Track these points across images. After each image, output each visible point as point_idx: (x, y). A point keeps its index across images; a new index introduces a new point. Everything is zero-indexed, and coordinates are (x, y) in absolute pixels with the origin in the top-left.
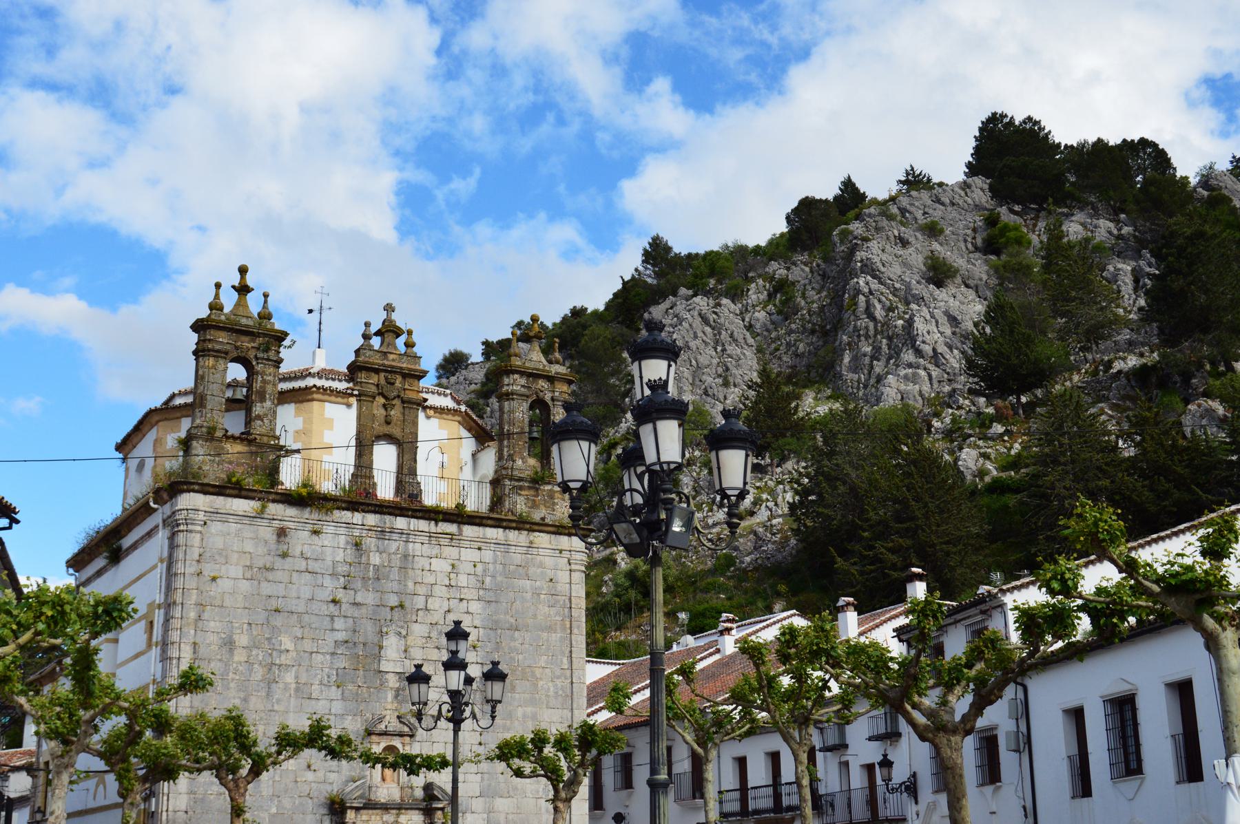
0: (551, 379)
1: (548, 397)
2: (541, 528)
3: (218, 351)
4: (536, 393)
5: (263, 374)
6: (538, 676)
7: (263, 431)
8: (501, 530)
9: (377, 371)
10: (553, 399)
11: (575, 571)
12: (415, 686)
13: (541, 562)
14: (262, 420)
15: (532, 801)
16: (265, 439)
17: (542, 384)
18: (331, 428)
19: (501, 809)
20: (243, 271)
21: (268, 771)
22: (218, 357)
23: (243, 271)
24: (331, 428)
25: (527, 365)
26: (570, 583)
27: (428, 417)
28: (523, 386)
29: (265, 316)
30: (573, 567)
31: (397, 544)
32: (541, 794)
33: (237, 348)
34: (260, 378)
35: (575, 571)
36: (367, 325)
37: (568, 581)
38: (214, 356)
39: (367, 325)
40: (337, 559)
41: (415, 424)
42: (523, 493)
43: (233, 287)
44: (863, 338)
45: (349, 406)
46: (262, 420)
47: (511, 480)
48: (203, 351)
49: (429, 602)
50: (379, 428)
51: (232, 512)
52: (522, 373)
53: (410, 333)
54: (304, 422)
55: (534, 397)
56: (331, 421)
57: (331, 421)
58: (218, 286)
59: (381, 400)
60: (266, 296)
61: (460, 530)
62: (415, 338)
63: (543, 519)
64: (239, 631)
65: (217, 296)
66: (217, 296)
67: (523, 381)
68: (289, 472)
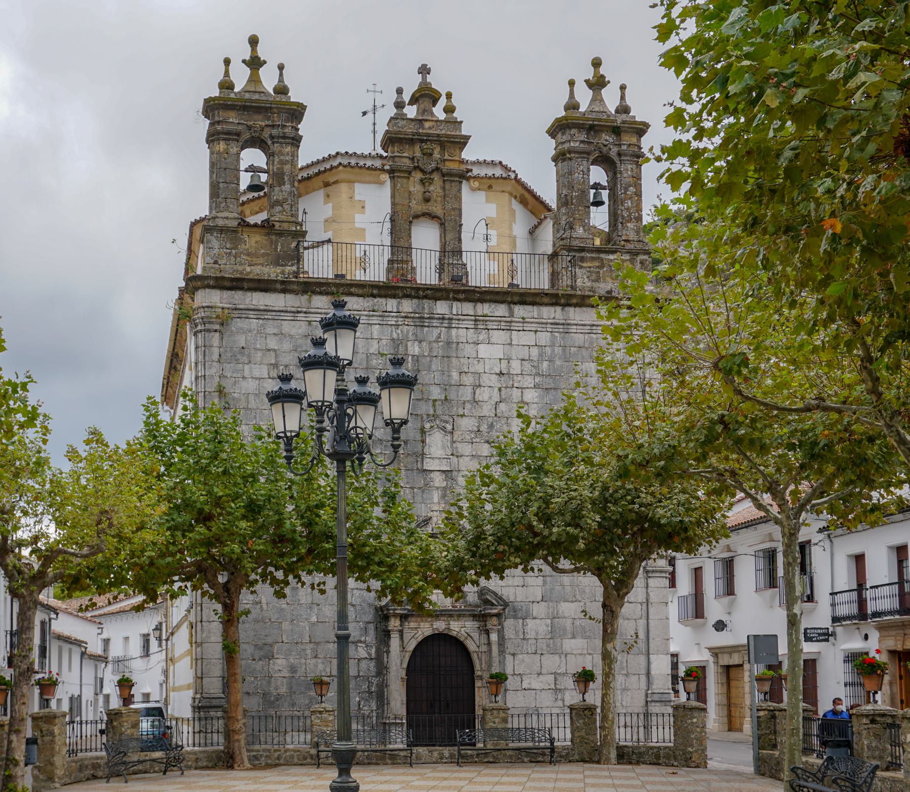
19: (566, 615)
36: (400, 91)
38: (225, 139)
39: (400, 91)
43: (244, 61)
50: (417, 206)
53: (449, 96)
60: (281, 67)
62: (454, 101)
65: (227, 74)
66: (227, 74)
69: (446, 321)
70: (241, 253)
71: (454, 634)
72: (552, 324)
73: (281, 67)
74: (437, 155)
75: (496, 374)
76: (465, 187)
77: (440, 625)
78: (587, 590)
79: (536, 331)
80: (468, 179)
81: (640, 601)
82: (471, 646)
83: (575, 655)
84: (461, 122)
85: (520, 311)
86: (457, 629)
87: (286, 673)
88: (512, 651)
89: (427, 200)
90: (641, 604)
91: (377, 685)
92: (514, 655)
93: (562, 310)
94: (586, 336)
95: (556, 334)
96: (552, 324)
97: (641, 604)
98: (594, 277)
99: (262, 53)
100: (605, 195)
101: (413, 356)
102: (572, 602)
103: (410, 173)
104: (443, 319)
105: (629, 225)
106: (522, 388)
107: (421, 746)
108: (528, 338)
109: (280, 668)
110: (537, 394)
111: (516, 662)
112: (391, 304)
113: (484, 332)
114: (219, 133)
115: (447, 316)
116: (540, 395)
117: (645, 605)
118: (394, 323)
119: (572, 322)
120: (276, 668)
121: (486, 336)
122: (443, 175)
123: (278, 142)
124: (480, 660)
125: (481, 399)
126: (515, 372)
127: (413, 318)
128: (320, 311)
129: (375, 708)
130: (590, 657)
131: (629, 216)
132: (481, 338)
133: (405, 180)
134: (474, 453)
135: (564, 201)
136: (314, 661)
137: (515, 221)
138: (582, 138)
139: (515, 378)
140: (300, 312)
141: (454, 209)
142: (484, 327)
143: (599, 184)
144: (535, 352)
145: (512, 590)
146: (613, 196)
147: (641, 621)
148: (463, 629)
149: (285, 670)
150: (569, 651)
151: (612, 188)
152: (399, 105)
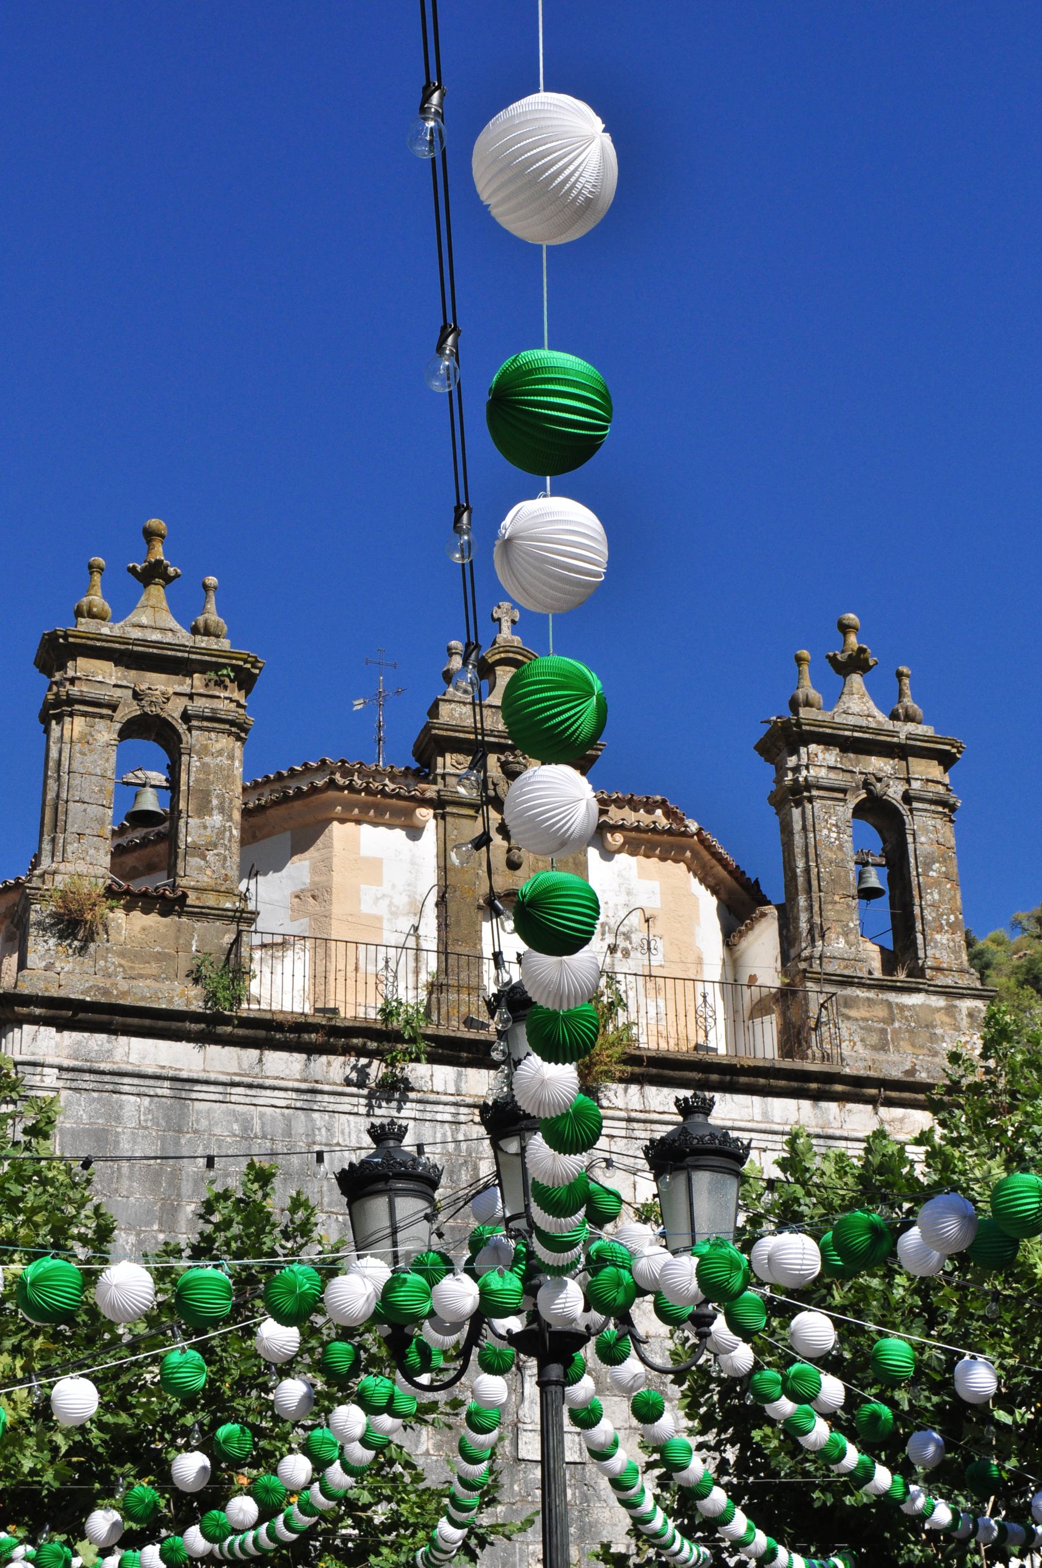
0: (900, 751)
1: (895, 792)
2: (976, 992)
4: (866, 785)
5: (205, 750)
7: (205, 879)
8: (806, 1104)
10: (907, 798)
12: (332, 1006)
14: (204, 857)
16: (211, 900)
21: (1035, 1265)
22: (94, 715)
25: (837, 720)
33: (137, 696)
34: (195, 762)
38: (85, 714)
42: (853, 1013)
45: (415, 832)
46: (204, 857)
47: (817, 981)
48: (58, 703)
51: (129, 1068)
52: (827, 740)
54: (314, 870)
55: (863, 794)
63: (912, 1072)
67: (831, 756)
68: (288, 987)
98: (874, 1039)
105: (938, 937)
118: (448, 1117)
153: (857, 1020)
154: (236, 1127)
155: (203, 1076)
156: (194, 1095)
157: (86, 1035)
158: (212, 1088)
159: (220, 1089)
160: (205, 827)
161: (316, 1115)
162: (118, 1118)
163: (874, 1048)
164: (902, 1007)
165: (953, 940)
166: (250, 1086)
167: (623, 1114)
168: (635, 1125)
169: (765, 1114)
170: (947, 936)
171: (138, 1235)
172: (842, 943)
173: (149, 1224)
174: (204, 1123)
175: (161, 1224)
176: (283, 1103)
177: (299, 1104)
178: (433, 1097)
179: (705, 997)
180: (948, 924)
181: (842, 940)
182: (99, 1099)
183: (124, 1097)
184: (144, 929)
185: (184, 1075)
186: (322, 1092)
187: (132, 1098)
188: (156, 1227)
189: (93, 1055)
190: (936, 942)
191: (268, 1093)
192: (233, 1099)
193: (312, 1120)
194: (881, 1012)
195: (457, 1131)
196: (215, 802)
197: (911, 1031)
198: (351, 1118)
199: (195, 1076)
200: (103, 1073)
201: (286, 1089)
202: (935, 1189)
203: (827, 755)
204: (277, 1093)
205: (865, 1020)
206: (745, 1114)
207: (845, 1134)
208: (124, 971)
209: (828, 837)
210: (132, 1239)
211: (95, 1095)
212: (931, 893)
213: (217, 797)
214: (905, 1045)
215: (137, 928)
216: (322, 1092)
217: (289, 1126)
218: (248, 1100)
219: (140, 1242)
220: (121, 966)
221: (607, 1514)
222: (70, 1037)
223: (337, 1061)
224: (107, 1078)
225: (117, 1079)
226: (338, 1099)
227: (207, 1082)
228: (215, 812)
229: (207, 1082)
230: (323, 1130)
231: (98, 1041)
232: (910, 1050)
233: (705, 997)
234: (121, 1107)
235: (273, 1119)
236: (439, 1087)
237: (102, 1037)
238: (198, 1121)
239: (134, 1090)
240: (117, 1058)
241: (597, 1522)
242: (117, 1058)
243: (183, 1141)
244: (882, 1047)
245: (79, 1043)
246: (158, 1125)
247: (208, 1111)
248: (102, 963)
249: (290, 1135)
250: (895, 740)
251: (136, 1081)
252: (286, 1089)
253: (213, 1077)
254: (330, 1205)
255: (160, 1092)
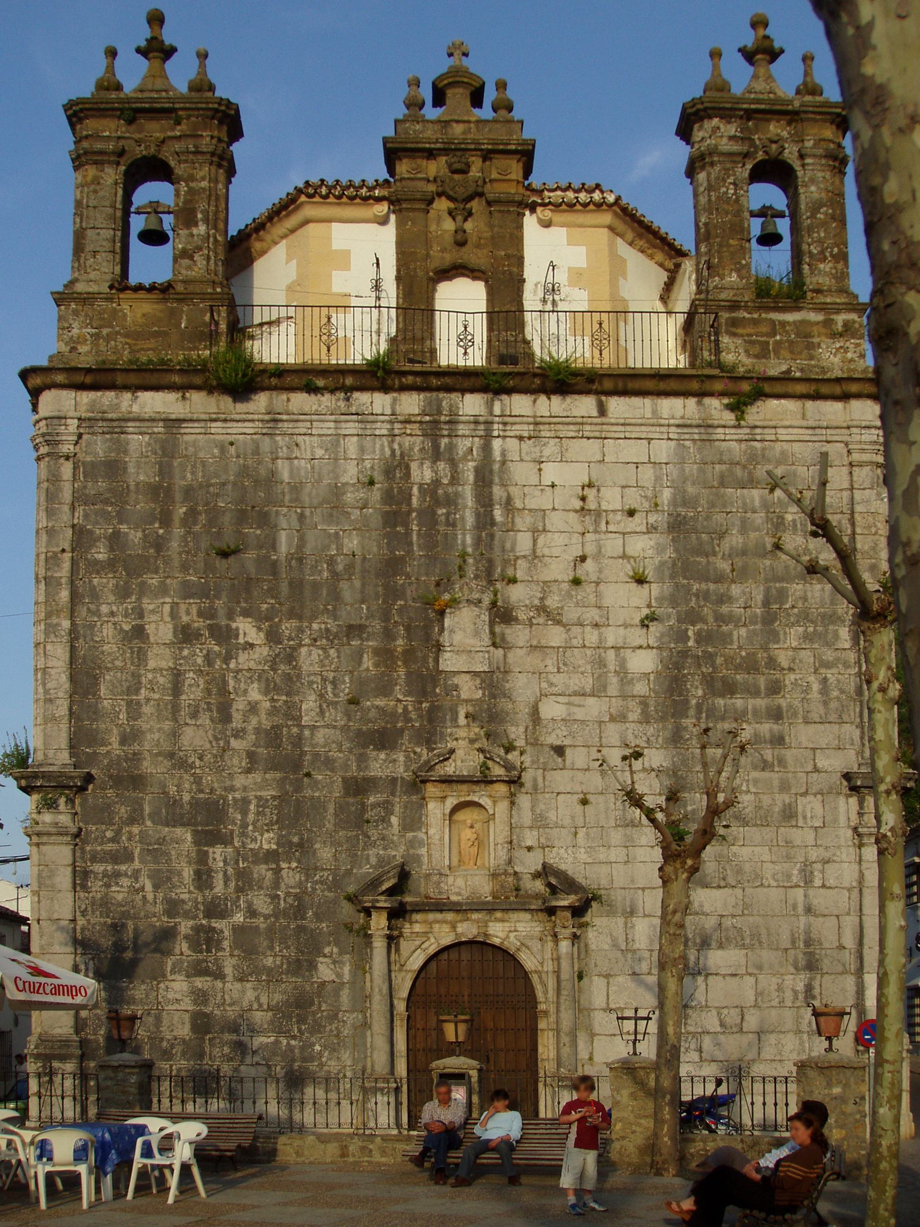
3: (101, 153)
6: (785, 664)
8: (692, 402)
9: (431, 154)
11: (861, 465)
13: (783, 453)
15: (775, 894)
17: (775, 129)
18: (346, 267)
19: (707, 909)
20: (156, 19)
23: (156, 19)
24: (346, 267)
26: (852, 489)
27: (547, 224)
28: (731, 138)
29: (202, 86)
30: (856, 457)
31: (468, 443)
32: (795, 879)
35: (861, 465)
36: (415, 83)
37: (846, 485)
38: (96, 163)
39: (415, 83)
40: (344, 479)
41: (517, 240)
43: (138, 50)
44: (725, 609)
49: (541, 541)
50: (440, 257)
53: (501, 86)
56: (346, 254)
57: (346, 254)
58: (112, 53)
59: (442, 205)
60: (203, 56)
61: (602, 410)
62: (511, 93)
63: (789, 371)
64: (154, 618)
65: (110, 69)
66: (110, 69)
67: (732, 129)
69: (482, 427)
70: (118, 333)
71: (497, 941)
72: (678, 426)
73: (203, 56)
74: (475, 172)
75: (576, 511)
76: (530, 222)
77: (467, 930)
78: (747, 867)
79: (649, 440)
80: (533, 208)
81: (846, 884)
82: (529, 961)
83: (724, 976)
84: (914, 443)
85: (617, 406)
86: (500, 934)
87: (188, 1004)
88: (604, 967)
89: (461, 244)
90: (849, 890)
91: (353, 1025)
92: (607, 976)
93: (699, 403)
94: (743, 445)
95: (687, 443)
96: (678, 426)
97: (849, 890)
98: (756, 349)
99: (168, 36)
100: (783, 226)
101: (421, 485)
102: (719, 887)
103: (431, 202)
104: (476, 423)
105: (822, 266)
106: (624, 534)
107: (535, 1049)
108: (634, 451)
109: (178, 996)
110: (652, 543)
111: (613, 988)
112: (380, 402)
113: (552, 442)
114: (86, 153)
115: (481, 419)
116: (658, 544)
117: (856, 891)
118: (385, 432)
119: (716, 423)
120: (171, 996)
121: (556, 449)
122: (489, 203)
123: (186, 161)
124: (545, 985)
125: (546, 552)
126: (611, 508)
127: (421, 422)
128: (250, 417)
129: (349, 1063)
130: (751, 980)
131: (822, 252)
132: (547, 452)
133: (421, 215)
134: (535, 643)
135: (703, 235)
136: (238, 985)
137: (624, 275)
138: (732, 133)
139: (611, 516)
140: (215, 420)
141: (508, 256)
142: (552, 434)
143: (771, 207)
144: (647, 475)
145: (605, 869)
146: (795, 229)
147: (847, 918)
148: (512, 935)
149: (187, 1000)
150: (713, 971)
151: (794, 215)
152: (414, 104)
153: (742, 336)
154: (216, 451)
155: (189, 416)
156: (183, 431)
157: (99, 394)
158: (196, 425)
159: (202, 424)
160: (192, 235)
161: (278, 438)
162: (126, 452)
163: (757, 357)
164: (783, 324)
165: (835, 268)
166: (225, 420)
167: (531, 420)
168: (542, 427)
169: (654, 412)
170: (830, 265)
171: (144, 531)
172: (734, 277)
173: (152, 523)
174: (191, 449)
175: (161, 523)
176: (252, 431)
177: (264, 431)
178: (371, 418)
179: (600, 324)
180: (832, 255)
181: (734, 275)
182: (111, 439)
183: (130, 436)
184: (144, 315)
185: (173, 417)
186: (282, 421)
187: (136, 437)
188: (157, 525)
189: (105, 408)
190: (820, 271)
191: (240, 424)
192: (213, 431)
193: (276, 442)
194: (764, 329)
195: (393, 441)
196: (200, 216)
197: (791, 343)
198: (307, 438)
199: (182, 416)
200: (112, 420)
201: (253, 421)
202: (470, 198)
203: (728, 126)
204: (246, 424)
205: (748, 335)
206: (639, 412)
207: (723, 423)
208: (130, 347)
209: (726, 193)
210: (139, 534)
211: (108, 436)
212: (818, 232)
213: (202, 212)
214: (784, 353)
215: (139, 315)
216: (282, 421)
217: (258, 447)
218: (224, 431)
219: (145, 536)
220: (127, 343)
221: (510, 706)
222: (86, 397)
223: (79, 290)
224: (116, 423)
225: (123, 424)
226: (296, 425)
227: (191, 420)
228: (200, 223)
229: (191, 420)
230: (285, 449)
231: (107, 398)
232: (788, 356)
233: (600, 324)
234: (128, 444)
235: (245, 443)
236: (377, 409)
237: (111, 394)
238: (186, 449)
239: (136, 430)
240: (123, 409)
241: (502, 711)
242: (123, 409)
243: (175, 464)
244: (764, 353)
245: (94, 401)
246: (156, 454)
247: (195, 442)
248: (113, 343)
249: (259, 454)
250: (790, 107)
251: (138, 424)
252: (253, 421)
253: (195, 417)
254: (290, 501)
255: (156, 430)
